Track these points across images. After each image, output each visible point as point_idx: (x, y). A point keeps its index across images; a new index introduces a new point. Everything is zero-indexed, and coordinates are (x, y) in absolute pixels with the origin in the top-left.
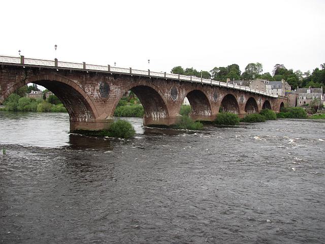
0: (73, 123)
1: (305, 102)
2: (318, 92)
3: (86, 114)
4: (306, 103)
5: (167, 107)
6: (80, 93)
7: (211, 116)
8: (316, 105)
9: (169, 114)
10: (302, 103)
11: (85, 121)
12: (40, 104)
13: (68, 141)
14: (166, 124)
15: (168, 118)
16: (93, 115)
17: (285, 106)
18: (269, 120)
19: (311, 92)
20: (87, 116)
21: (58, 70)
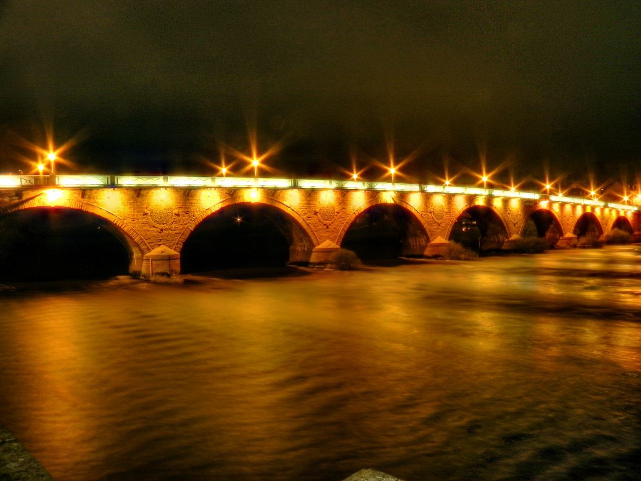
3: (304, 241)
20: (306, 244)
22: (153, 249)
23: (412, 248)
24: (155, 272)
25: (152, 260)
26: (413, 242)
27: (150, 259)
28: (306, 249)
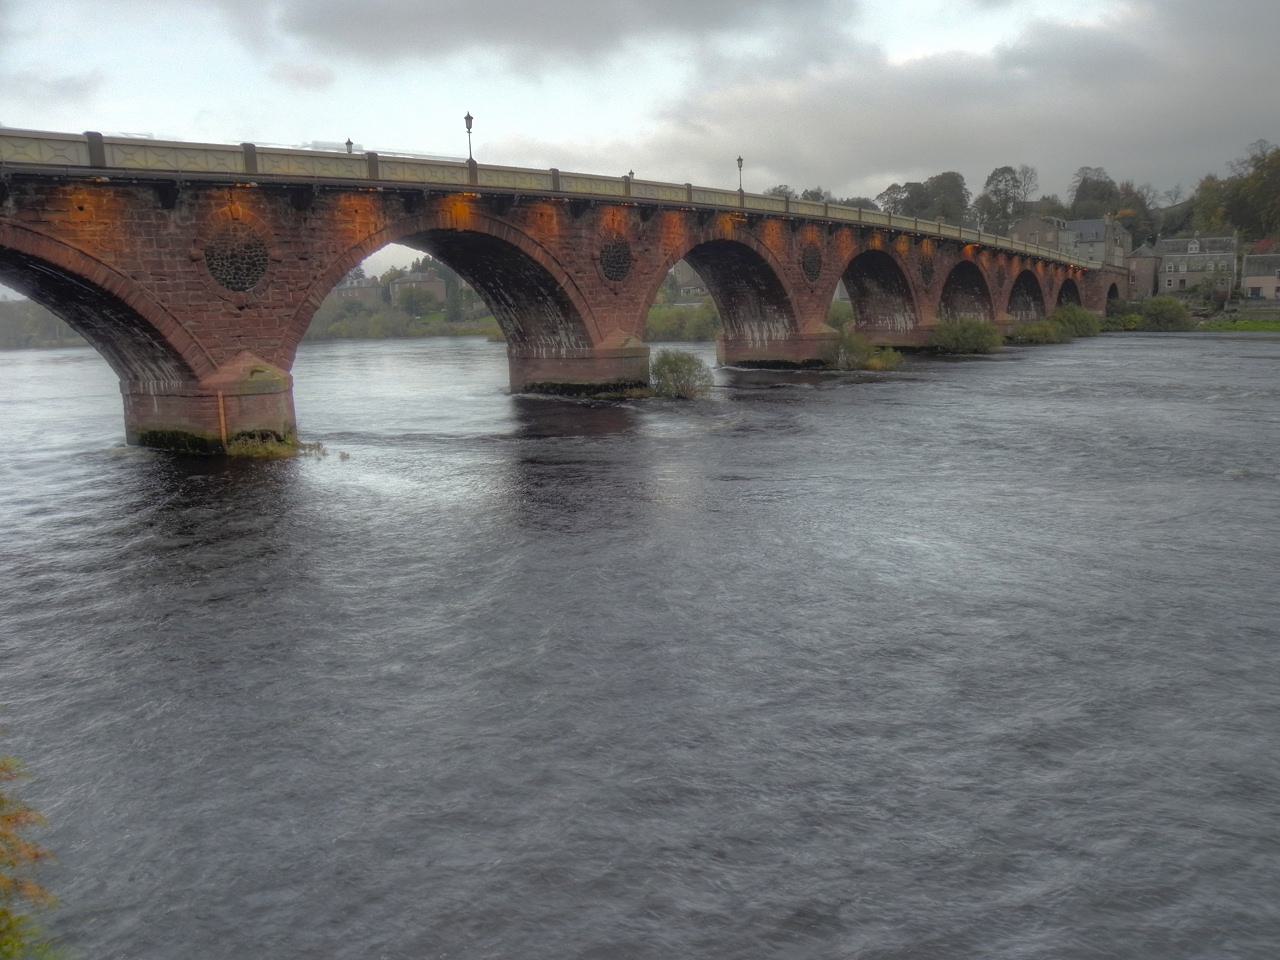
0: (520, 361)
1: (1182, 282)
2: (1225, 248)
3: (562, 333)
4: (1189, 284)
5: (794, 304)
6: (543, 270)
7: (916, 329)
8: (1220, 287)
9: (800, 326)
10: (1175, 286)
11: (558, 358)
12: (376, 317)
13: (509, 428)
14: (789, 357)
15: (795, 340)
16: (585, 337)
17: (1122, 294)
18: (1080, 336)
19: (1202, 249)
20: (564, 339)
21: (567, 200)
22: (221, 364)
23: (750, 346)
24: (237, 430)
25: (224, 397)
26: (752, 332)
27: (220, 393)
28: (563, 351)
